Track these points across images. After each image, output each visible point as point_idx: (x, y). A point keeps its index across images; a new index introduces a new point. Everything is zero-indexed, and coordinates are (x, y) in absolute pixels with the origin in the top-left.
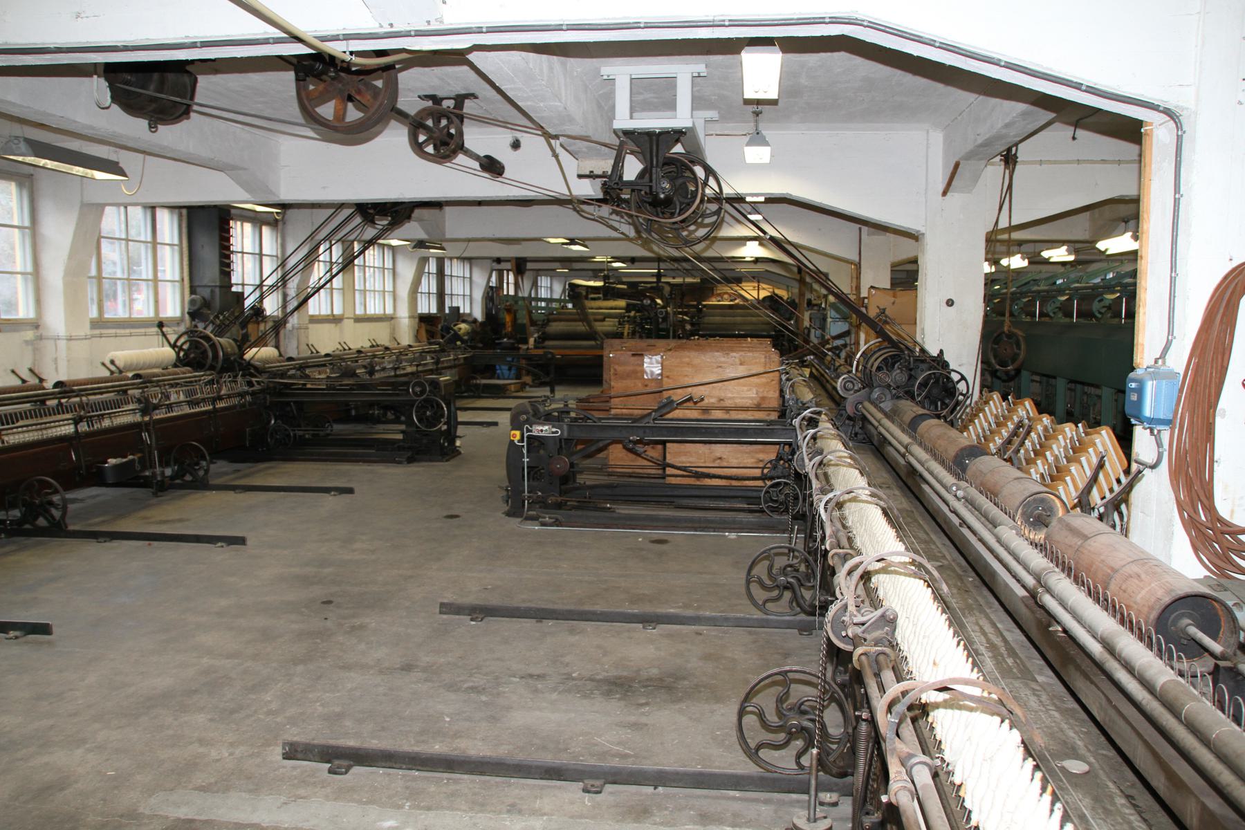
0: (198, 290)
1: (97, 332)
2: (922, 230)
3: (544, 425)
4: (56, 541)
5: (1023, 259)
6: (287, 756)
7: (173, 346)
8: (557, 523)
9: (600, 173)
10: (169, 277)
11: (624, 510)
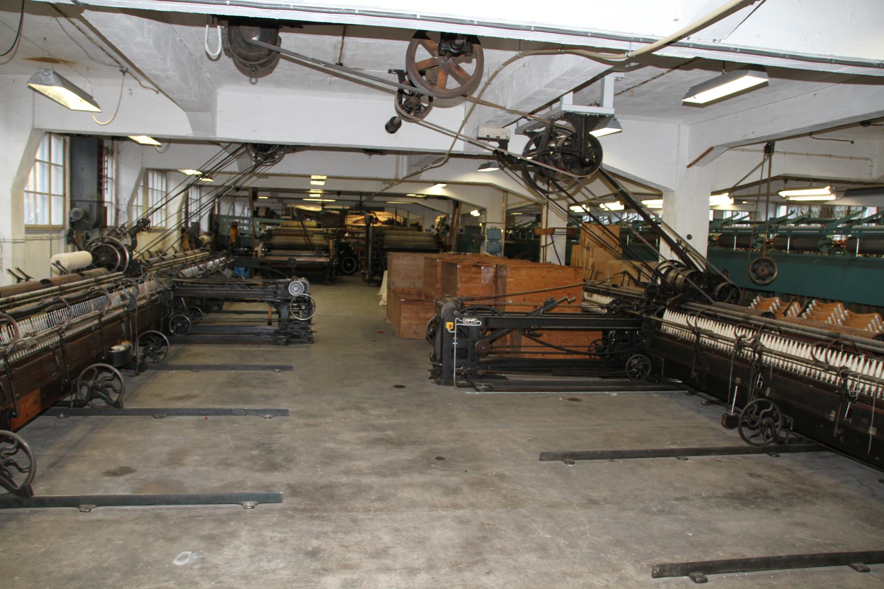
0: (77, 204)
1: (32, 236)
2: (673, 189)
3: (471, 318)
4: (118, 419)
5: (621, 204)
6: (655, 576)
8: (490, 389)
9: (494, 137)
11: (513, 377)
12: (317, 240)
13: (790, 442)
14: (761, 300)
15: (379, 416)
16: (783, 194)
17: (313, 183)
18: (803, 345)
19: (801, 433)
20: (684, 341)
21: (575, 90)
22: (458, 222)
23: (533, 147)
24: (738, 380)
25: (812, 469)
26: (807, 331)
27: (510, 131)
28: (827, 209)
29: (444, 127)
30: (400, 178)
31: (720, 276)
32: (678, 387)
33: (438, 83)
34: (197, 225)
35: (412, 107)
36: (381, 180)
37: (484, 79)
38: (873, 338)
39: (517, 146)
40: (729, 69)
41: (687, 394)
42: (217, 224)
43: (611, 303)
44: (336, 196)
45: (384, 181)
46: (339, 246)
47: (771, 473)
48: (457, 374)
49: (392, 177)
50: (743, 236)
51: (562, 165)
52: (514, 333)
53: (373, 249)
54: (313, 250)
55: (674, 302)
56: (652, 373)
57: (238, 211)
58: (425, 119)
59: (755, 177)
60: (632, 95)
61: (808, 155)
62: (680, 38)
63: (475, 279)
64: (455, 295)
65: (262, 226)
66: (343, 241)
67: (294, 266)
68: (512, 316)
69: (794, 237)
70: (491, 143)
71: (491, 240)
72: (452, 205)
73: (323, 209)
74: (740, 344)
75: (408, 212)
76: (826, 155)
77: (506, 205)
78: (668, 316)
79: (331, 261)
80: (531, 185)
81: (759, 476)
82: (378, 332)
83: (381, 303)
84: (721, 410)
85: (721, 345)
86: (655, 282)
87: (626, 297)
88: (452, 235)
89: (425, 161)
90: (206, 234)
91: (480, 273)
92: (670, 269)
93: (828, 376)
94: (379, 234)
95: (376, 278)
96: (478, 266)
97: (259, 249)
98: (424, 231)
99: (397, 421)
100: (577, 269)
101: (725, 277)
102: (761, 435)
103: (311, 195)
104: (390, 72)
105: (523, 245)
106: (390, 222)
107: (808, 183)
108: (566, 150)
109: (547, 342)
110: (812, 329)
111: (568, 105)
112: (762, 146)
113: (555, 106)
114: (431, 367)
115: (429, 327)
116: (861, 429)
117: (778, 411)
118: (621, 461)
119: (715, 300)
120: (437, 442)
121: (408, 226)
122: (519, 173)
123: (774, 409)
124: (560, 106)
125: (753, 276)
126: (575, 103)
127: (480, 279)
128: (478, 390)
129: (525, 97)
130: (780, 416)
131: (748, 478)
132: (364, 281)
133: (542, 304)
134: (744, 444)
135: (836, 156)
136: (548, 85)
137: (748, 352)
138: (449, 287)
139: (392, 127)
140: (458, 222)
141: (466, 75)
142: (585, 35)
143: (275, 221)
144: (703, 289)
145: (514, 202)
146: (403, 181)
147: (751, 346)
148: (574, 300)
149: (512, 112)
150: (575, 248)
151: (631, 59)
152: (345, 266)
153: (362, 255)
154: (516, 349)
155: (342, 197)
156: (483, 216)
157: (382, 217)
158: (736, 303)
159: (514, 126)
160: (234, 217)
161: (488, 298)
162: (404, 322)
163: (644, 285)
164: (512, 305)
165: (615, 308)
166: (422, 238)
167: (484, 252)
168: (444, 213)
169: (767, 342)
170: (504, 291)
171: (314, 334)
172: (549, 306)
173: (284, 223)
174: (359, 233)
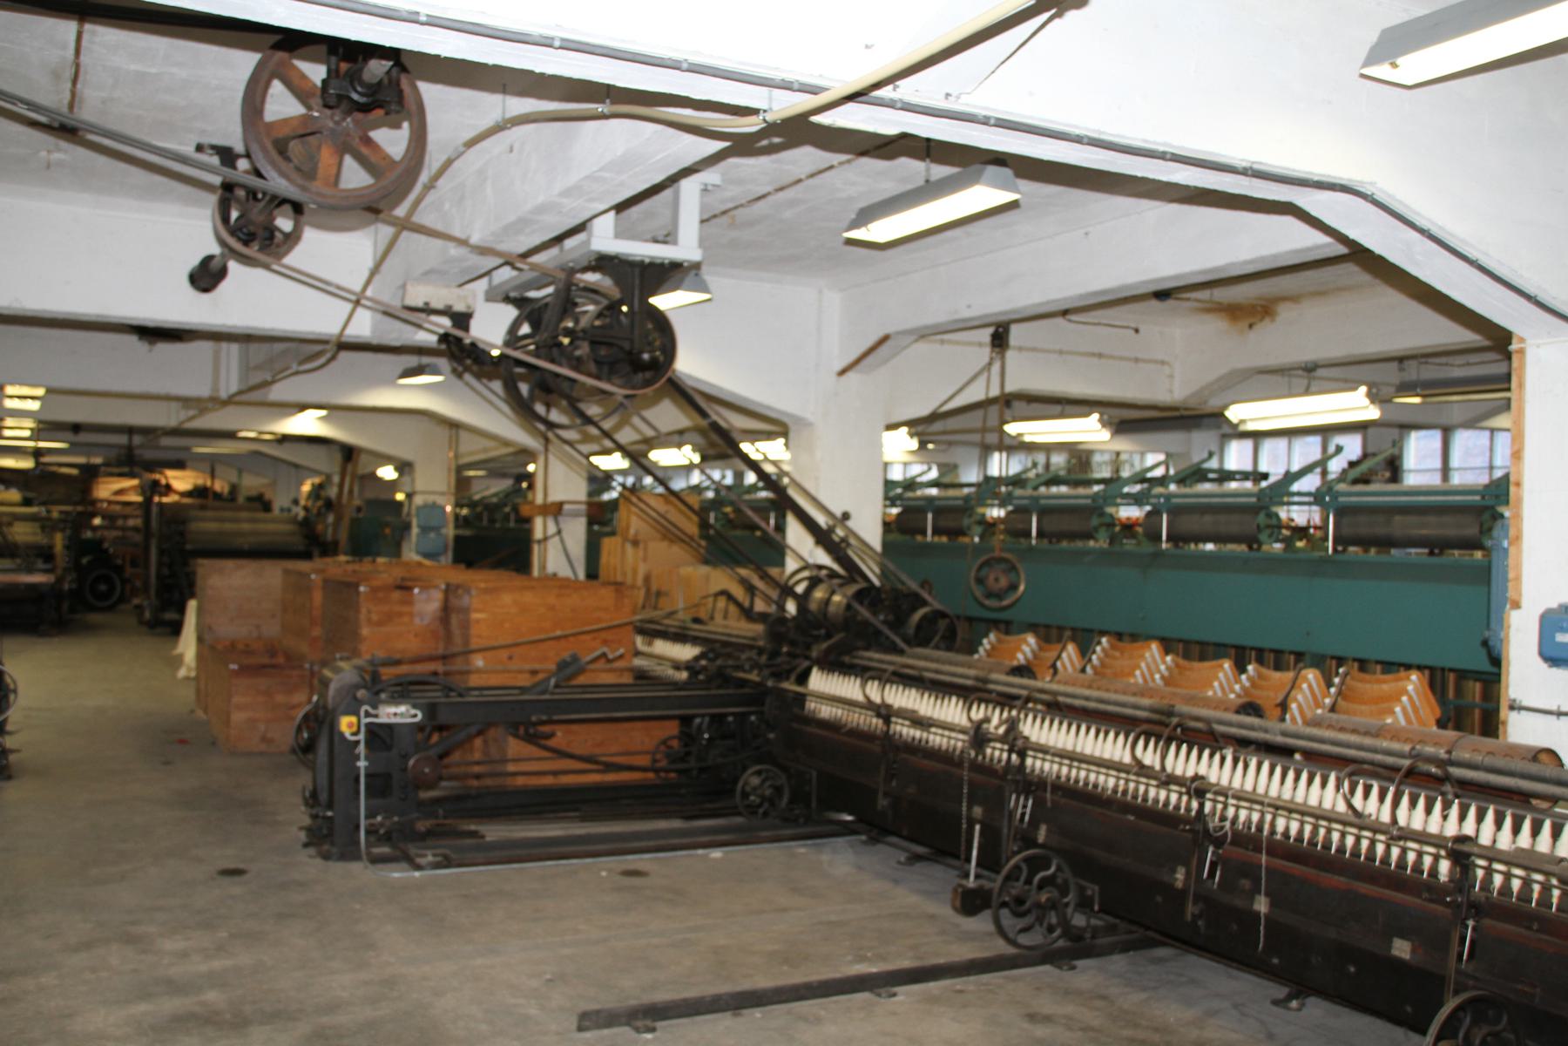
3: (398, 704)
8: (447, 863)
11: (494, 832)
13: (1093, 937)
14: (999, 641)
15: (184, 955)
16: (1012, 428)
17: (9, 404)
18: (1106, 733)
19: (1116, 916)
20: (856, 733)
21: (621, 208)
22: (351, 492)
23: (525, 329)
24: (978, 811)
25: (1144, 989)
26: (1375, 751)
27: (474, 296)
28: (1080, 456)
29: (325, 279)
30: (223, 395)
31: (916, 595)
32: (845, 830)
33: (321, 172)
35: (254, 225)
36: (177, 399)
37: (424, 178)
38: (1238, 712)
39: (492, 327)
40: (968, 161)
41: (864, 843)
43: (697, 659)
44: (70, 436)
45: (186, 401)
46: (78, 546)
47: (1070, 1009)
48: (368, 832)
49: (204, 391)
50: (941, 510)
51: (592, 367)
52: (492, 733)
53: (161, 552)
55: (828, 651)
56: (791, 802)
58: (287, 260)
59: (976, 394)
60: (732, 225)
61: (1061, 352)
62: (877, 85)
63: (400, 614)
64: (355, 653)
66: (89, 534)
68: (490, 696)
69: (1044, 512)
70: (434, 318)
71: (425, 530)
72: (338, 457)
73: (38, 463)
74: (979, 737)
75: (240, 472)
76: (1093, 355)
77: (456, 456)
78: (819, 682)
79: (59, 580)
80: (523, 409)
81: (1047, 1019)
82: (175, 741)
83: (182, 673)
84: (941, 876)
85: (937, 739)
86: (782, 608)
87: (726, 644)
88: (339, 519)
89: (281, 357)
91: (410, 603)
92: (814, 582)
93: (1163, 794)
94: (175, 518)
95: (170, 616)
96: (404, 587)
98: (276, 511)
99: (228, 963)
100: (619, 586)
101: (926, 596)
102: (1037, 927)
103: (7, 433)
104: (200, 148)
105: (494, 537)
106: (199, 492)
107: (1058, 408)
108: (596, 337)
109: (564, 747)
110: (1113, 697)
111: (605, 238)
112: (986, 335)
113: (569, 243)
114: (307, 821)
115: (299, 729)
116: (1239, 902)
117: (1068, 873)
118: (757, 1013)
119: (908, 642)
120: (333, 1007)
121: (241, 500)
122: (497, 385)
123: (1059, 869)
124: (588, 242)
125: (978, 593)
126: (619, 234)
127: (411, 615)
128: (419, 868)
129: (512, 218)
130: (1072, 881)
131: (1026, 1025)
132: (142, 622)
133: (553, 667)
134: (1010, 950)
135: (1112, 357)
136: (567, 193)
137: (997, 753)
138: (341, 635)
139: (206, 277)
140: (351, 492)
141: (386, 157)
142: (674, 65)
144: (885, 622)
145: (472, 449)
146: (226, 403)
147: (1003, 739)
148: (621, 657)
149: (483, 251)
150: (608, 544)
151: (771, 129)
153: (134, 564)
154: (499, 768)
155: (84, 437)
156: (406, 479)
157: (181, 481)
158: (949, 649)
159: (482, 284)
161: (431, 659)
162: (238, 717)
163: (763, 617)
164: (483, 671)
165: (704, 668)
166: (273, 527)
167: (410, 554)
168: (316, 472)
169: (1035, 730)
170: (466, 641)
171: (12, 758)
172: (569, 671)
174: (126, 517)
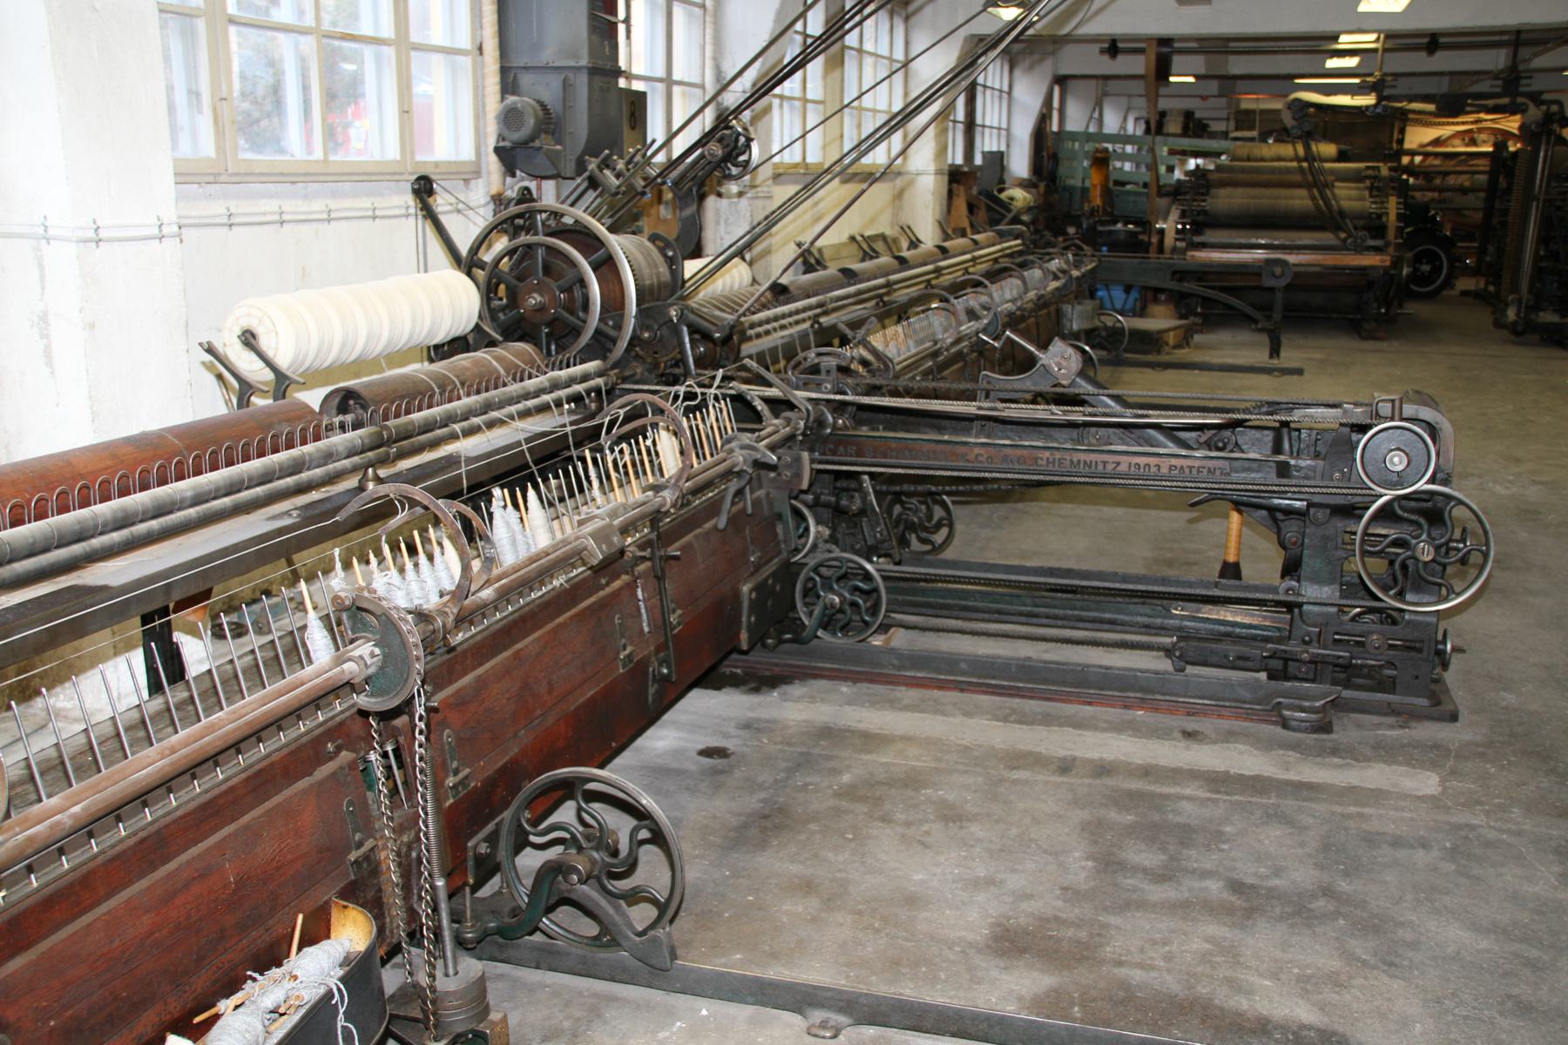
0: (525, 80)
7: (468, 264)
10: (438, 37)
12: (1349, 197)
34: (997, 160)
42: (1055, 158)
54: (1337, 228)
57: (1112, 122)
65: (1175, 160)
67: (1283, 282)
73: (1380, 99)
79: (1397, 263)
90: (1023, 184)
97: (1169, 225)
132: (1499, 324)
143: (1214, 145)
152: (1437, 270)
160: (1101, 137)
173: (1243, 149)
174: (1447, 174)
